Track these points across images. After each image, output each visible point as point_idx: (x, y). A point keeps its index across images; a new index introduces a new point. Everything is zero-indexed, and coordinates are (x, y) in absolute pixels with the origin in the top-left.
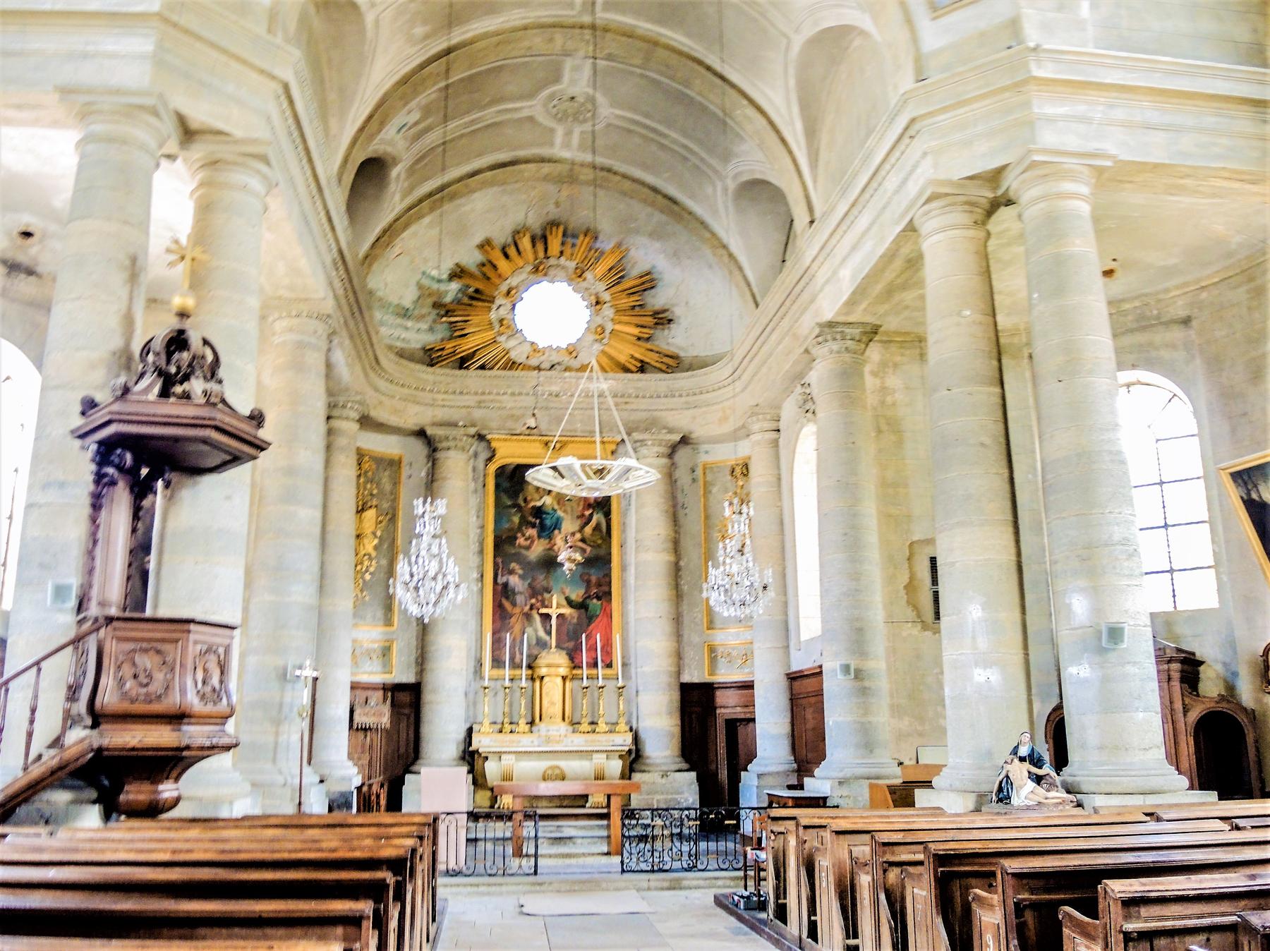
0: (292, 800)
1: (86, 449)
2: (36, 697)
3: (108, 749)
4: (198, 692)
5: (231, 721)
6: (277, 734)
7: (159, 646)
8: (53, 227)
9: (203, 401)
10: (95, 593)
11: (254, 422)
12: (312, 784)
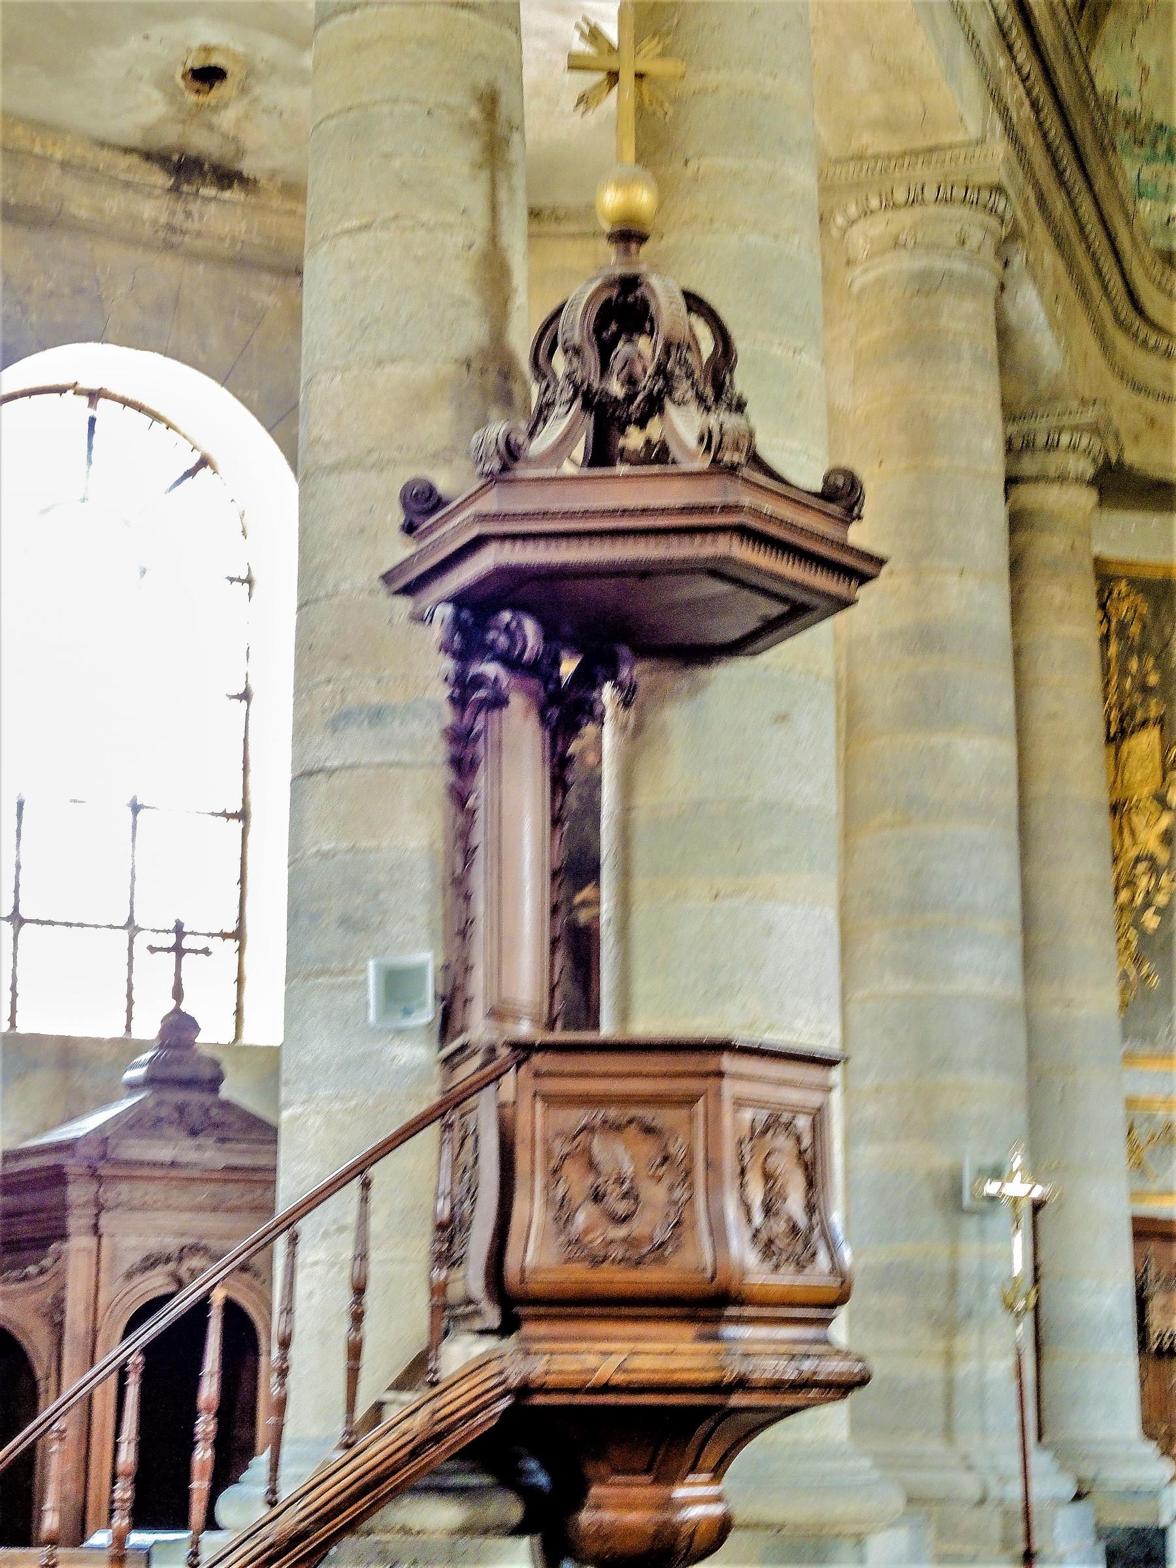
0: (1007, 1544)
1: (421, 618)
2: (362, 1257)
3: (543, 1390)
4: (756, 1234)
5: (842, 1315)
6: (949, 1358)
7: (647, 1114)
8: (269, 48)
9: (702, 463)
10: (478, 984)
11: (834, 508)
12: (1056, 1502)
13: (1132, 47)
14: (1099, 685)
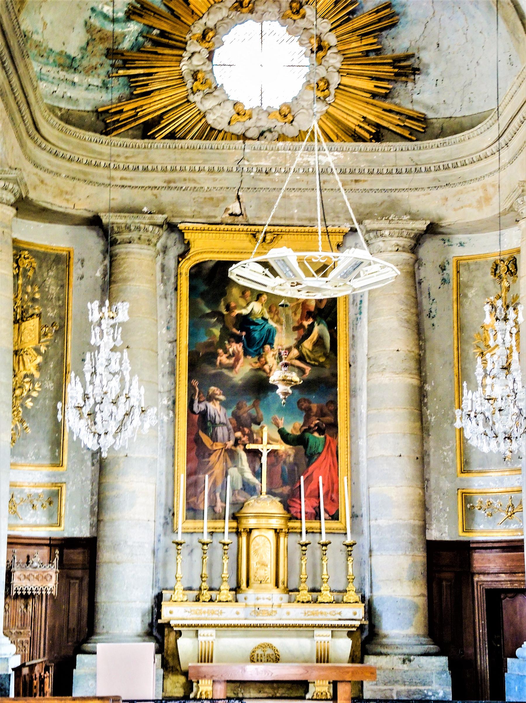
13: (40, 13)
14: (12, 296)
